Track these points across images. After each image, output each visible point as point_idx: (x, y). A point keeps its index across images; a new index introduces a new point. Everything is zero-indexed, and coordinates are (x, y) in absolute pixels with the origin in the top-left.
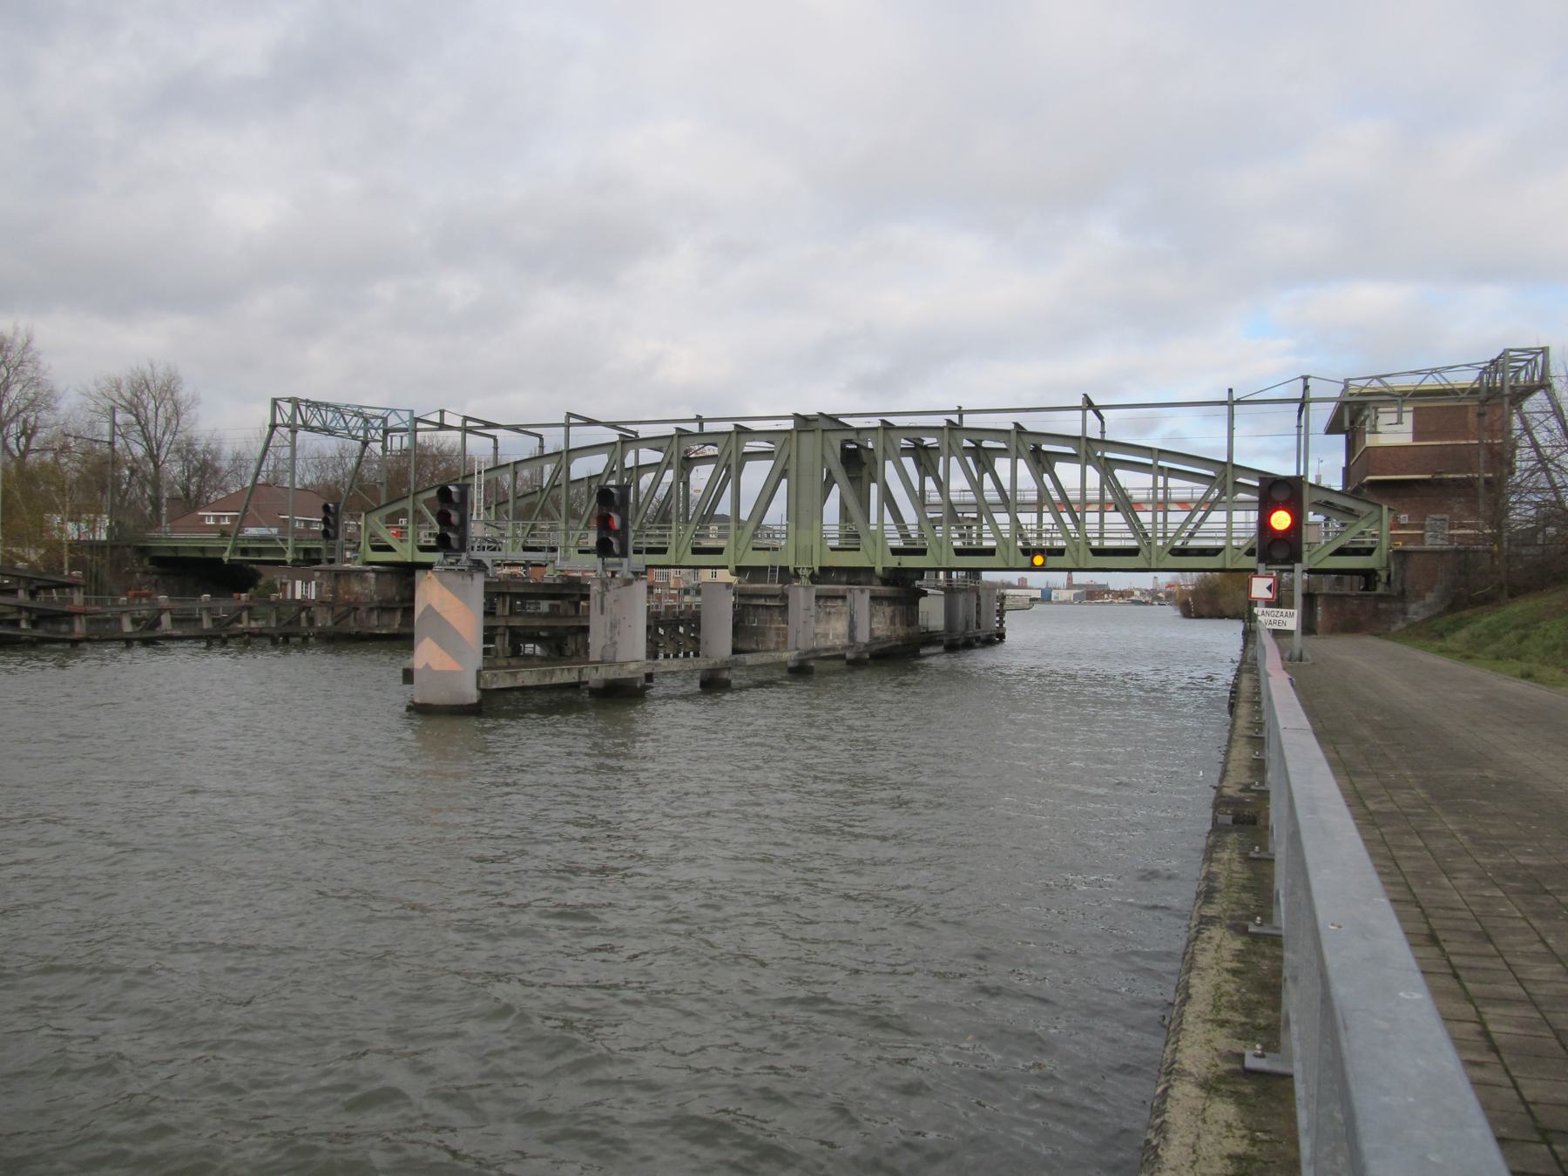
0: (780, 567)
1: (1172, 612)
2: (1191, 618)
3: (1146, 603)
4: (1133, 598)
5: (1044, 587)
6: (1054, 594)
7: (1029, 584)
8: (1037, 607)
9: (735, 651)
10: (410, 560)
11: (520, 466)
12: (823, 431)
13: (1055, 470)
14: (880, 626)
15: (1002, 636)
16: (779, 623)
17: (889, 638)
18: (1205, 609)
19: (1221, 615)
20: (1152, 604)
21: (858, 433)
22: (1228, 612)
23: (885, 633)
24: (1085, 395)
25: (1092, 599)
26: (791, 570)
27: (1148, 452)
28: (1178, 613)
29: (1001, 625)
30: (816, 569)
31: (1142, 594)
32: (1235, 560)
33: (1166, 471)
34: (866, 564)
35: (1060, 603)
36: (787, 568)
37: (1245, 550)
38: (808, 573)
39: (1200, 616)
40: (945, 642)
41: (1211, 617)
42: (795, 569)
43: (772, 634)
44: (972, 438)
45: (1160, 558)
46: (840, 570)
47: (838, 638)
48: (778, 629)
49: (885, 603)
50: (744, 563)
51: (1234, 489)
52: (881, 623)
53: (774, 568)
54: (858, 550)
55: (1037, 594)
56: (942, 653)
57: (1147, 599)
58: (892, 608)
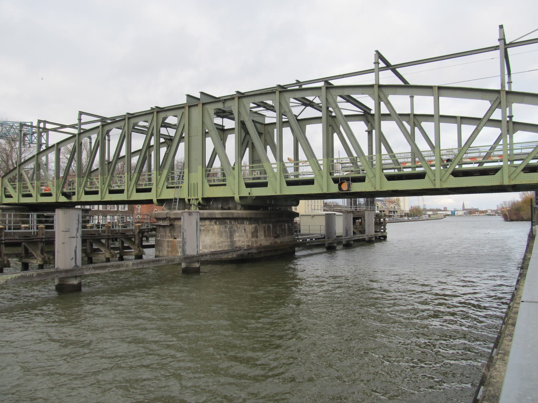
0: (180, 199)
1: (500, 219)
2: (508, 221)
3: (493, 215)
4: (487, 213)
5: (453, 210)
6: (456, 213)
7: (448, 209)
8: (448, 218)
9: (376, 232)
10: (17, 202)
11: (60, 145)
12: (203, 104)
13: (410, 147)
14: (242, 239)
15: (385, 237)
16: (169, 238)
17: (249, 248)
18: (514, 217)
19: (522, 220)
20: (495, 215)
21: (224, 103)
22: (525, 218)
23: (246, 244)
24: (377, 52)
25: (471, 214)
26: (186, 200)
27: (454, 120)
28: (503, 219)
29: (385, 231)
30: (200, 200)
31: (492, 211)
32: (513, 177)
33: (459, 119)
34: (230, 195)
35: (458, 216)
36: (183, 200)
37: (522, 167)
38: (196, 203)
39: (512, 220)
40: (326, 245)
41: (517, 220)
42: (189, 200)
43: (165, 245)
44: (296, 97)
45: (444, 180)
46: (216, 199)
47: (206, 248)
48: (168, 242)
49: (246, 223)
50: (163, 197)
51: (513, 126)
52: (243, 236)
53: (176, 199)
54: (225, 185)
55: (450, 213)
56: (325, 252)
57: (493, 213)
58: (254, 226)
